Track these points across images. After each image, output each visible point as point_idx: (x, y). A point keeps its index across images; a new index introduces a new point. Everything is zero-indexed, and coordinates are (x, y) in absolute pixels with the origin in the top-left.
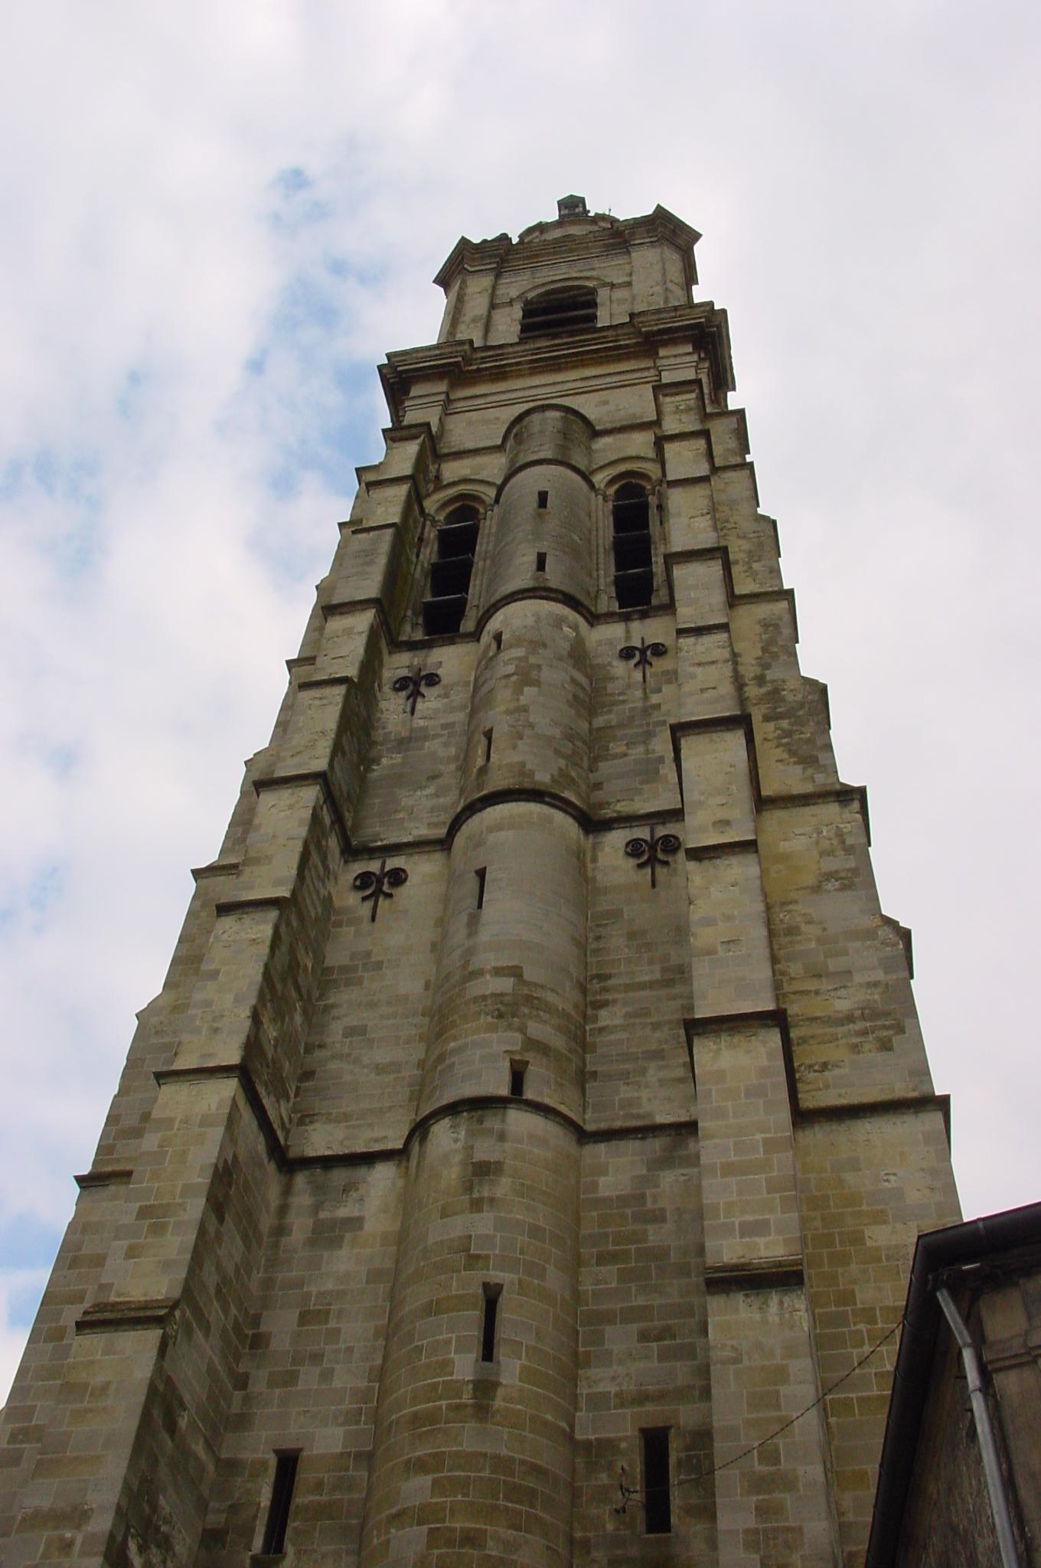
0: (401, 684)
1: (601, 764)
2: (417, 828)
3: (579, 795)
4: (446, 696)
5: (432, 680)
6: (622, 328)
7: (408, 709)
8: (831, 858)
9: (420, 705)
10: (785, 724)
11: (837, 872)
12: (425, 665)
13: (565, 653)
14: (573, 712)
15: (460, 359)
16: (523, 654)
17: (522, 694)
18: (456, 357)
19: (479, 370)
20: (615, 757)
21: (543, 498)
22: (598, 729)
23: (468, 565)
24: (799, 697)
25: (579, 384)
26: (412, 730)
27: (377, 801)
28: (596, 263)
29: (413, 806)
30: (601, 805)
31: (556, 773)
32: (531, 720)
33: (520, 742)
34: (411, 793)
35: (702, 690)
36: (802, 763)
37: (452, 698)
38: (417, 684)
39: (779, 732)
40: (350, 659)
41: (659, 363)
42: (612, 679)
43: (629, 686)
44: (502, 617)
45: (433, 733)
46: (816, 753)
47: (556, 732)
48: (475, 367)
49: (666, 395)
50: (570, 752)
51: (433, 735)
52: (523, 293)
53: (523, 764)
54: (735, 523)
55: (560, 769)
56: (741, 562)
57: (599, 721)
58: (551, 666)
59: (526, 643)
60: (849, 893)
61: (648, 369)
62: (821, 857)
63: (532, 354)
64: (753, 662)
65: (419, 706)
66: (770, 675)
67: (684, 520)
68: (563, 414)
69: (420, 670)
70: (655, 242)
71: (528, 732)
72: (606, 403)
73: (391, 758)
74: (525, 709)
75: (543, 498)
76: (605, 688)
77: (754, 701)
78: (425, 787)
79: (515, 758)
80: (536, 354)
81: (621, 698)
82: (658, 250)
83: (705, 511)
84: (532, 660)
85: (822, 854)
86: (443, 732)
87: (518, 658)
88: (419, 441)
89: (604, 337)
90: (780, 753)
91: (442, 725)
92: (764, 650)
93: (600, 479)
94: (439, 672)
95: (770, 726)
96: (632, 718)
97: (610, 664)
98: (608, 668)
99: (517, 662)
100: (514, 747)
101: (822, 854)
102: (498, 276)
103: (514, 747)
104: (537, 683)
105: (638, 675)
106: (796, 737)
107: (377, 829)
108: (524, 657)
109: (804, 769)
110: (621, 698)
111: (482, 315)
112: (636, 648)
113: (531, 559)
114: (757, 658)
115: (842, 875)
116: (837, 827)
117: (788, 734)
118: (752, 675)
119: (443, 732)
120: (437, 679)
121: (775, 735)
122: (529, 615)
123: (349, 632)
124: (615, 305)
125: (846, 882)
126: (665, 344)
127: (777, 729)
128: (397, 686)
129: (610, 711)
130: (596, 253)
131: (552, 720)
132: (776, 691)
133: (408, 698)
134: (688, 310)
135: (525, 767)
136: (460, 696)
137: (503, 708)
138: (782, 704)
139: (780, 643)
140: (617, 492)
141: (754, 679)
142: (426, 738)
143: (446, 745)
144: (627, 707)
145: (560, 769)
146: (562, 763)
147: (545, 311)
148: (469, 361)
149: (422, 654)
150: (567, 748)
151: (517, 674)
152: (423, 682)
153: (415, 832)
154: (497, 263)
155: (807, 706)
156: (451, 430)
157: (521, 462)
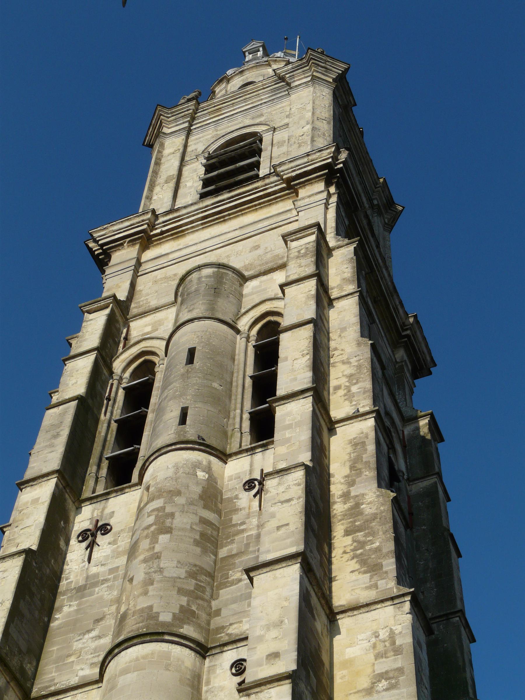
0: (84, 535)
1: (221, 592)
2: (82, 669)
3: (199, 627)
4: (114, 542)
5: (105, 529)
6: (269, 177)
7: (86, 559)
8: (384, 659)
9: (97, 554)
10: (360, 535)
11: (387, 672)
12: (102, 516)
13: (196, 497)
14: (198, 550)
15: (145, 226)
16: (162, 505)
17: (157, 542)
18: (142, 225)
19: (162, 233)
20: (233, 583)
21: (192, 352)
22: (223, 559)
23: (143, 417)
24: (373, 510)
25: (237, 233)
26: (87, 578)
27: (55, 648)
28: (265, 109)
29: (81, 648)
30: (221, 629)
31: (177, 611)
32: (162, 565)
33: (150, 588)
34: (81, 637)
35: (278, 528)
36: (369, 572)
37: (119, 544)
38: (94, 536)
39: (355, 544)
40: (33, 528)
41: (299, 204)
42: (237, 510)
43: (248, 516)
44: (152, 470)
45: (102, 578)
46: (379, 561)
47: (182, 573)
48: (158, 231)
49: (292, 241)
50: (192, 588)
51: (103, 580)
52: (206, 148)
53: (151, 607)
54: (342, 350)
55: (182, 606)
56: (343, 386)
57: (223, 552)
58: (183, 512)
59: (165, 494)
60: (394, 692)
61: (290, 210)
62: (376, 659)
63: (202, 212)
64: (342, 481)
65: (95, 555)
66: (354, 492)
67: (289, 362)
68: (216, 270)
69: (97, 521)
70: (309, 81)
71: (157, 577)
72: (257, 247)
73: (70, 605)
74: (157, 556)
75: (192, 352)
76: (231, 519)
77: (339, 518)
78: (92, 630)
79: (143, 603)
80: (205, 211)
81: (242, 527)
82: (311, 89)
83: (305, 352)
84: (168, 509)
85: (378, 656)
86: (110, 577)
87: (157, 509)
88: (107, 311)
89: (256, 188)
90: (354, 565)
91: (110, 570)
92: (352, 468)
93: (243, 324)
94: (112, 522)
95: (349, 540)
96: (247, 545)
97: (237, 497)
98: (235, 501)
99: (156, 513)
100: (146, 593)
101: (378, 656)
102: (189, 132)
103: (146, 593)
104: (169, 530)
105: (256, 503)
106: (368, 548)
107: (53, 674)
108: (161, 507)
109: (371, 577)
110: (242, 527)
111: (174, 175)
112: (256, 480)
113: (176, 413)
114: (346, 477)
115: (391, 675)
116: (391, 629)
117: (361, 544)
118: (340, 493)
119: (110, 577)
120: (109, 527)
121: (352, 547)
122: (170, 466)
123: (36, 501)
124: (275, 149)
125: (393, 681)
126: (303, 184)
127: (354, 541)
128: (80, 538)
129: (232, 542)
130: (266, 98)
131: (179, 562)
132: (357, 505)
133: (87, 549)
134: (318, 154)
135: (152, 610)
136: (124, 542)
137: (141, 557)
138: (360, 517)
139: (364, 460)
140: (259, 332)
141: (341, 496)
142: (95, 584)
143: (110, 588)
144: (245, 535)
145: (182, 606)
146: (184, 601)
147: (223, 164)
148: (152, 226)
149: (99, 506)
150: (191, 585)
151: (156, 525)
152: (99, 532)
153: (81, 673)
154: (189, 121)
155: (379, 516)
156: (141, 291)
157: (181, 321)
